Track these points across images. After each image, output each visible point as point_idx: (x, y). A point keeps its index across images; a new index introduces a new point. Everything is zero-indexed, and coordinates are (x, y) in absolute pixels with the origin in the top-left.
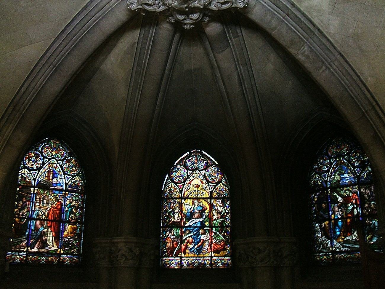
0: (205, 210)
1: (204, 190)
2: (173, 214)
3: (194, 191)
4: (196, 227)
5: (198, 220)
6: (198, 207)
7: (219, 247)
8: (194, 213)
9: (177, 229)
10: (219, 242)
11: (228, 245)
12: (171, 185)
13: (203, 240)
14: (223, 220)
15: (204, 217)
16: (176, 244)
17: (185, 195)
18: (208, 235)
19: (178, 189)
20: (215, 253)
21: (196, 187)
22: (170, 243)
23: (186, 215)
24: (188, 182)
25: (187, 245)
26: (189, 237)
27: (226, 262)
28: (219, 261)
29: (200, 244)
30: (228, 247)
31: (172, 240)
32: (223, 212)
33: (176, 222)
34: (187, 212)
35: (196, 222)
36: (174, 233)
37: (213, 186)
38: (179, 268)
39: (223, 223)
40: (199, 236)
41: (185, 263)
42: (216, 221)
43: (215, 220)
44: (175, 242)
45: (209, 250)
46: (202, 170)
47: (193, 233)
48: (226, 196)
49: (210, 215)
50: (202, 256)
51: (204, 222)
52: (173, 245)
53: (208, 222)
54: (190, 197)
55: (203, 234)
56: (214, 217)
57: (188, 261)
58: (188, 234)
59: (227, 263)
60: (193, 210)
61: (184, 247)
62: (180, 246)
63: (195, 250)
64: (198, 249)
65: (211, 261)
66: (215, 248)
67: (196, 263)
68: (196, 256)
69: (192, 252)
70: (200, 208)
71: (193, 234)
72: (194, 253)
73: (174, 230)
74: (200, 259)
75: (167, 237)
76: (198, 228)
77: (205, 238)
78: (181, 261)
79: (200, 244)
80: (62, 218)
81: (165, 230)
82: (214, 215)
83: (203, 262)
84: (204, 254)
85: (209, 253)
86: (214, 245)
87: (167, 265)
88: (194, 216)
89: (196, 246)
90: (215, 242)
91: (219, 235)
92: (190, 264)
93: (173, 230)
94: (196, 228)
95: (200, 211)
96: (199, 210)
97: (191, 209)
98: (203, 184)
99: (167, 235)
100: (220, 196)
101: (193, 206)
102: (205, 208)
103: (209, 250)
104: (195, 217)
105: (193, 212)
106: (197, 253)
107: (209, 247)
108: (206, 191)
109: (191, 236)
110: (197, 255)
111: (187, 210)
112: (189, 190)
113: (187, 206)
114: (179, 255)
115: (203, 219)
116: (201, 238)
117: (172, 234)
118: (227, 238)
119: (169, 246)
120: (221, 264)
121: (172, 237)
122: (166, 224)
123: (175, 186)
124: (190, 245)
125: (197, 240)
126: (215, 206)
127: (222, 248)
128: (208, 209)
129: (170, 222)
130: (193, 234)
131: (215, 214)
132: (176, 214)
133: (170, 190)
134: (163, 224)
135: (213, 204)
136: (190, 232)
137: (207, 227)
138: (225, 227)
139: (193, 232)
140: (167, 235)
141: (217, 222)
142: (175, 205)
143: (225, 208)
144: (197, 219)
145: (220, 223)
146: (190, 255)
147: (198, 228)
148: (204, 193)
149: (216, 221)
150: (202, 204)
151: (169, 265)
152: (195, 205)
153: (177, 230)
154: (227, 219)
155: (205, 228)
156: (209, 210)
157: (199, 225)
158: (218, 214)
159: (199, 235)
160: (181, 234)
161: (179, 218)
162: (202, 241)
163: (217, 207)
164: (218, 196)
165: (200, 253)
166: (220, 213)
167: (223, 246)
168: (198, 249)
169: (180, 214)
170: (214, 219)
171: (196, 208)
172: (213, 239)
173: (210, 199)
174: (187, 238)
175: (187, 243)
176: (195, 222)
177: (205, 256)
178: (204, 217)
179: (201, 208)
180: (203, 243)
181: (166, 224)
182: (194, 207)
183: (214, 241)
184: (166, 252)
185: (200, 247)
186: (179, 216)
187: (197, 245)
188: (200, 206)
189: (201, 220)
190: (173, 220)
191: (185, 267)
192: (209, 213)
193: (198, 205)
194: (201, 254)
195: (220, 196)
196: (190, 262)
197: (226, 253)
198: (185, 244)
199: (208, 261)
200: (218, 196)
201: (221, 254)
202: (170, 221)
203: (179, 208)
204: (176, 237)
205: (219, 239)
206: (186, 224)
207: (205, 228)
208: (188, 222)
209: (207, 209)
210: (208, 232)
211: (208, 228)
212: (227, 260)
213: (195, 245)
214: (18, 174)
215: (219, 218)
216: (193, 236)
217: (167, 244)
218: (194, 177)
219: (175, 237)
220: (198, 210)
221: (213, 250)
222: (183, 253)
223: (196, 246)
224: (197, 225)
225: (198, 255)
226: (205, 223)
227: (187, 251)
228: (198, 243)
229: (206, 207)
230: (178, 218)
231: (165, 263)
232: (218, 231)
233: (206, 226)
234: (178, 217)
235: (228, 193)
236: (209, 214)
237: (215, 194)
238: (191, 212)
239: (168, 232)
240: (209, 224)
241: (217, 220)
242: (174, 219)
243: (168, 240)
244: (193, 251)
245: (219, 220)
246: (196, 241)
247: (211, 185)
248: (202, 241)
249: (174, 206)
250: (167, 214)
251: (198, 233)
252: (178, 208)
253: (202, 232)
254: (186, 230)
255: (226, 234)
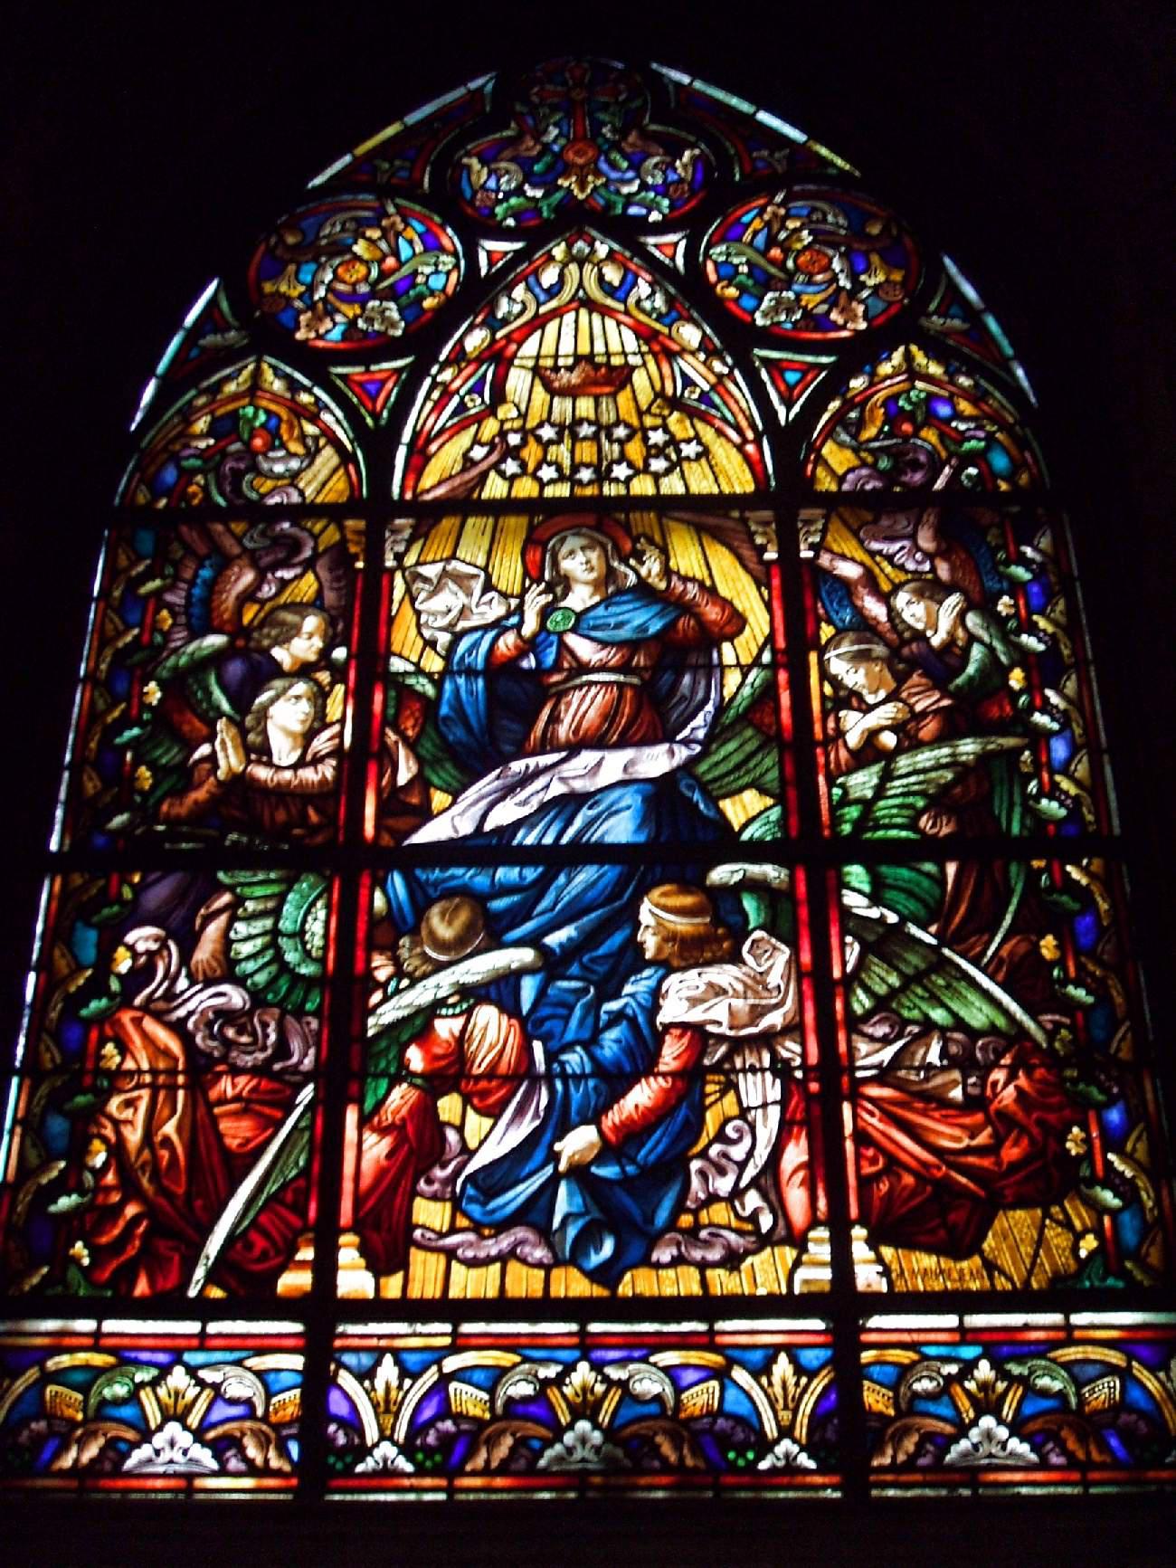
0: (711, 638)
1: (691, 413)
2: (243, 697)
3: (547, 433)
4: (584, 852)
5: (614, 764)
6: (607, 601)
7: (949, 1136)
8: (540, 672)
9: (289, 883)
10: (962, 1062)
11: (1101, 1108)
12: (246, 373)
13: (698, 1034)
14: (983, 758)
15: (699, 725)
16: (246, 1106)
17: (428, 480)
18: (778, 963)
19: (333, 418)
20: (907, 1242)
21: (572, 392)
22: (161, 1086)
23: (430, 705)
24: (476, 341)
25: (425, 1112)
26: (471, 995)
27: (1104, 1391)
28: (984, 1371)
29: (641, 1096)
30: (1113, 1141)
31: (186, 1038)
32: (977, 652)
33: (281, 794)
34: (447, 672)
35: (579, 785)
36: (227, 942)
37: (806, 369)
38: (274, 1490)
39: (988, 799)
40: (638, 986)
41: (386, 1408)
42: (887, 776)
43: (869, 752)
44: (235, 1071)
45: (796, 1198)
46: (659, 229)
47: (533, 940)
48: (988, 475)
49: (785, 698)
50: (685, 1283)
51: (704, 788)
52: (201, 1126)
53: (763, 791)
54: (495, 488)
55: (690, 953)
56: (855, 726)
57: (431, 1376)
58: (460, 949)
59: (1119, 1407)
60: (530, 645)
61: (377, 1148)
62: (328, 1146)
63: (565, 1201)
64: (608, 1172)
65: (848, 1373)
66: (894, 1165)
67: (586, 1408)
68: (571, 1284)
69: (502, 1227)
70: (639, 618)
71: (526, 955)
72: (540, 1253)
73: (239, 901)
74: (646, 1347)
75: (125, 1000)
76: (611, 873)
77: (717, 1015)
78: (317, 1382)
79: (641, 1096)
80: (290, 1497)
81: (106, 898)
82: (846, 699)
83: (701, 1397)
84: (715, 1254)
85: (799, 1242)
86: (874, 1122)
87: (65, 1434)
88: (554, 719)
89: (579, 1142)
90: (884, 1075)
91: (943, 965)
92: (475, 1433)
93: (226, 898)
94: (586, 875)
95: (630, 646)
96: (624, 633)
97: (498, 626)
98: (671, 356)
99: (124, 964)
100: (918, 477)
101: (535, 601)
102: (713, 613)
103: (796, 1198)
104: (563, 731)
105: (529, 663)
106: (588, 1239)
107: (795, 1154)
108: (707, 434)
109: (500, 990)
110: (594, 1276)
111: (444, 639)
112: (479, 419)
113: (450, 598)
114: (295, 1281)
115: (682, 753)
116: (663, 1017)
117: (204, 952)
118: (1070, 1006)
119: (134, 1136)
120: (1016, 1428)
121: (201, 1001)
122: (119, 820)
123: (294, 386)
124: (476, 1124)
125: (590, 1043)
126: (845, 585)
127: (1011, 1153)
128: (759, 622)
129: (179, 792)
130: (526, 955)
131: (854, 677)
132: (278, 684)
133: (226, 427)
134: (84, 816)
135: (825, 560)
136: (492, 933)
137: (756, 852)
138: (1022, 849)
139: (529, 926)
140: (124, 964)
141: (896, 786)
142: (284, 584)
143: (1004, 605)
144: (588, 757)
145: (939, 801)
146: (469, 1283)
147: (611, 873)
148: (690, 450)
149: (887, 776)
150: (667, 572)
151: (92, 1451)
152: (561, 584)
153: (281, 899)
154: (1039, 739)
155: (723, 874)
156: (770, 639)
157: (621, 829)
158: (901, 679)
159: (634, 957)
160: (344, 955)
161: (322, 743)
162: (671, 1054)
163: (886, 598)
164: (889, 477)
165: (653, 1241)
166: (950, 657)
167: (1023, 1130)
168: (608, 1172)
169: (339, 689)
170: (853, 739)
171: (580, 616)
172: (854, 1024)
173: (767, 514)
174: (432, 1010)
175: (435, 1083)
176: (557, 789)
177: (723, 1282)
178: (699, 725)
179: (641, 619)
180: (691, 1079)
181: (119, 820)
182: (545, 613)
183: (871, 1055)
184: (72, 1225)
185: (649, 1151)
186: (334, 709)
187: (595, 1120)
188: (644, 591)
189: (656, 761)
190: (230, 760)
191: (387, 1473)
192: (773, 666)
193: (610, 575)
194: (664, 1254)
195: (918, 477)
196: (468, 1399)
197: (1089, 1244)
198: (400, 1098)
199: (783, 1367)
200: (881, 475)
201: (1006, 1261)
202: (184, 777)
203: (331, 622)
204: (258, 998)
205: (960, 1024)
206: (425, 814)
207: (723, 874)
208: (455, 795)
209: (737, 622)
210: (770, 927)
211: (771, 872)
212: (1115, 1358)
213: (559, 1121)
214: (301, 1429)
215: (929, 729)
216: (529, 988)
217: (106, 1096)
218: (553, 292)
219: (236, 997)
220: (604, 644)
221: (865, 1183)
222: (349, 1255)
223: (579, 1142)
224: (590, 824)
225: (607, 1275)
226: (713, 801)
227: (430, 1214)
228: (616, 1081)
229: (726, 604)
230: (309, 736)
231: (42, 1411)
232: (933, 913)
233: (730, 845)
234: (319, 722)
235: (1021, 443)
236: (767, 693)
237: (837, 456)
238: (499, 671)
239: (143, 937)
240: (775, 814)
241: (903, 763)
242: (263, 752)
243: (124, 1049)
244: (535, 1213)
245: (925, 758)
246: (575, 1060)
247: (775, 367)
248: (671, 1054)
249: (268, 590)
250: (154, 693)
251: (617, 939)
252: (312, 622)
253: (682, 925)
254: (422, 900)
255: (1048, 947)
